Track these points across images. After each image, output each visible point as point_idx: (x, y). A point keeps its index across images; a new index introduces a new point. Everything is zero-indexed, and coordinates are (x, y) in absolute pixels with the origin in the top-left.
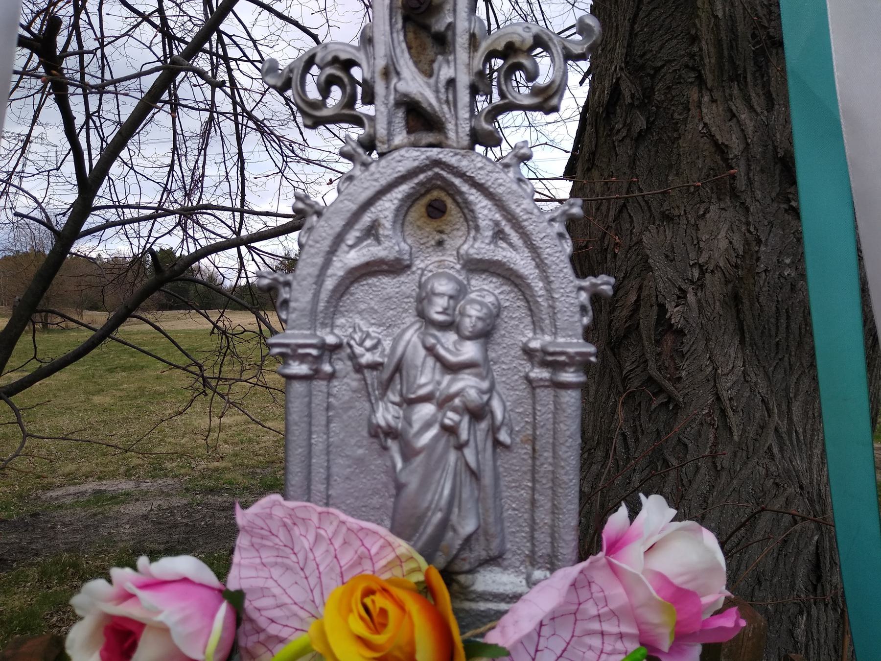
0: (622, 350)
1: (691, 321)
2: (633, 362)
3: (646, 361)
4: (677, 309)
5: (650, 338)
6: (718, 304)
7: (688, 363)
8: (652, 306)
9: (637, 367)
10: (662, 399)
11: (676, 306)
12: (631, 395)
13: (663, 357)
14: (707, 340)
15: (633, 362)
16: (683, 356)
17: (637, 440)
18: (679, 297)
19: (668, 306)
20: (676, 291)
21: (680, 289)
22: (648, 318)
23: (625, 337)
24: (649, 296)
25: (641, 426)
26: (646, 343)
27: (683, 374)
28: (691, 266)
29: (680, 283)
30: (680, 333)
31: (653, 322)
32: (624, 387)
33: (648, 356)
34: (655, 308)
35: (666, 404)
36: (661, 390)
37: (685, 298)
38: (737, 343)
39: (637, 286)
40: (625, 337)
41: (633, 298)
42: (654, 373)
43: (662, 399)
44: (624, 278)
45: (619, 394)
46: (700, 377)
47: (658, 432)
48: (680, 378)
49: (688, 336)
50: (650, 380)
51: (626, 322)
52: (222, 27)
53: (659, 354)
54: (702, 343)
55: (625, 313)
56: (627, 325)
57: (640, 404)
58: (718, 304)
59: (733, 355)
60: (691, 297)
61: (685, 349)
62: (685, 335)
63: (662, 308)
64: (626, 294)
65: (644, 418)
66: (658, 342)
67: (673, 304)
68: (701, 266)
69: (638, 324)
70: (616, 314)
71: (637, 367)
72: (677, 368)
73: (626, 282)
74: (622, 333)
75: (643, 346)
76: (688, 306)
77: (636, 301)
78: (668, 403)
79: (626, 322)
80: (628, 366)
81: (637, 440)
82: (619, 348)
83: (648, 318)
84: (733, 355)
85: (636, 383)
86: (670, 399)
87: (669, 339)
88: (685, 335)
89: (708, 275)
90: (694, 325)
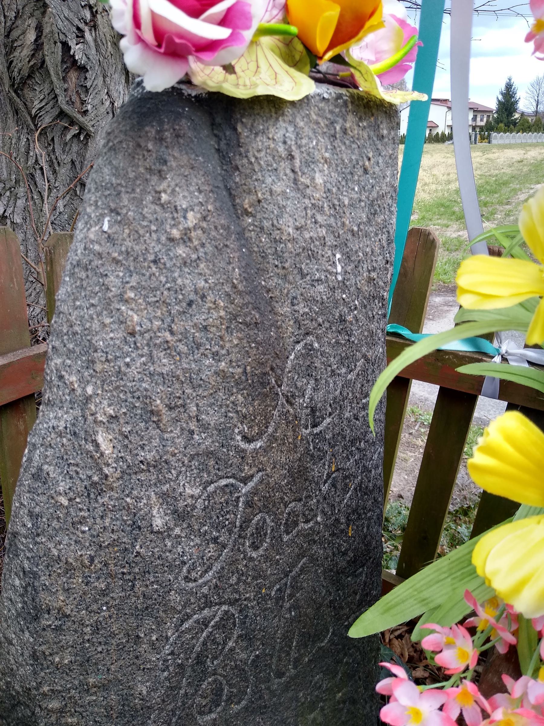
0: (26, 91)
1: (91, 57)
2: (41, 101)
3: (56, 96)
4: (78, 46)
5: (58, 75)
6: (109, 44)
7: (91, 96)
8: (55, 43)
9: (46, 105)
10: (74, 130)
11: (77, 44)
12: (43, 133)
13: (70, 93)
14: (104, 77)
15: (41, 101)
16: (87, 91)
17: (55, 172)
18: (77, 37)
19: (70, 43)
20: (74, 29)
21: (78, 29)
22: (53, 57)
23: (30, 77)
24: (52, 32)
25: (56, 159)
26: (54, 79)
27: (89, 107)
28: (82, 7)
29: (76, 22)
30: (83, 69)
31: (60, 58)
32: (36, 126)
33: (58, 91)
34: (59, 45)
35: (77, 136)
36: (72, 122)
37: (83, 37)
38: (123, 81)
39: (34, 25)
40: (30, 77)
41: (31, 36)
42: (65, 107)
43: (74, 130)
44: (15, 17)
45: (30, 132)
46: (102, 110)
47: (73, 162)
48: (87, 111)
49: (90, 72)
50: (62, 114)
51: (29, 62)
52: (419, 12)
53: (66, 90)
54: (101, 79)
55: (26, 52)
56: (32, 63)
57: (53, 139)
58: (109, 44)
59: (122, 92)
60: (87, 35)
61: (88, 84)
62: (87, 71)
63: (66, 47)
64: (24, 33)
65: (58, 151)
66: (64, 79)
67: (75, 42)
68: (91, 8)
69: (43, 62)
70: (16, 54)
71: (46, 105)
72: (83, 102)
73: (19, 22)
74: (25, 72)
75: (52, 82)
76: (87, 44)
77: (36, 40)
78: (79, 134)
79: (29, 62)
80: (37, 105)
81: (55, 172)
82: (22, 90)
83: (53, 57)
84: (122, 92)
85: (47, 120)
86: (81, 129)
87: (73, 75)
88: (87, 71)
89: (99, 16)
90: (94, 62)
